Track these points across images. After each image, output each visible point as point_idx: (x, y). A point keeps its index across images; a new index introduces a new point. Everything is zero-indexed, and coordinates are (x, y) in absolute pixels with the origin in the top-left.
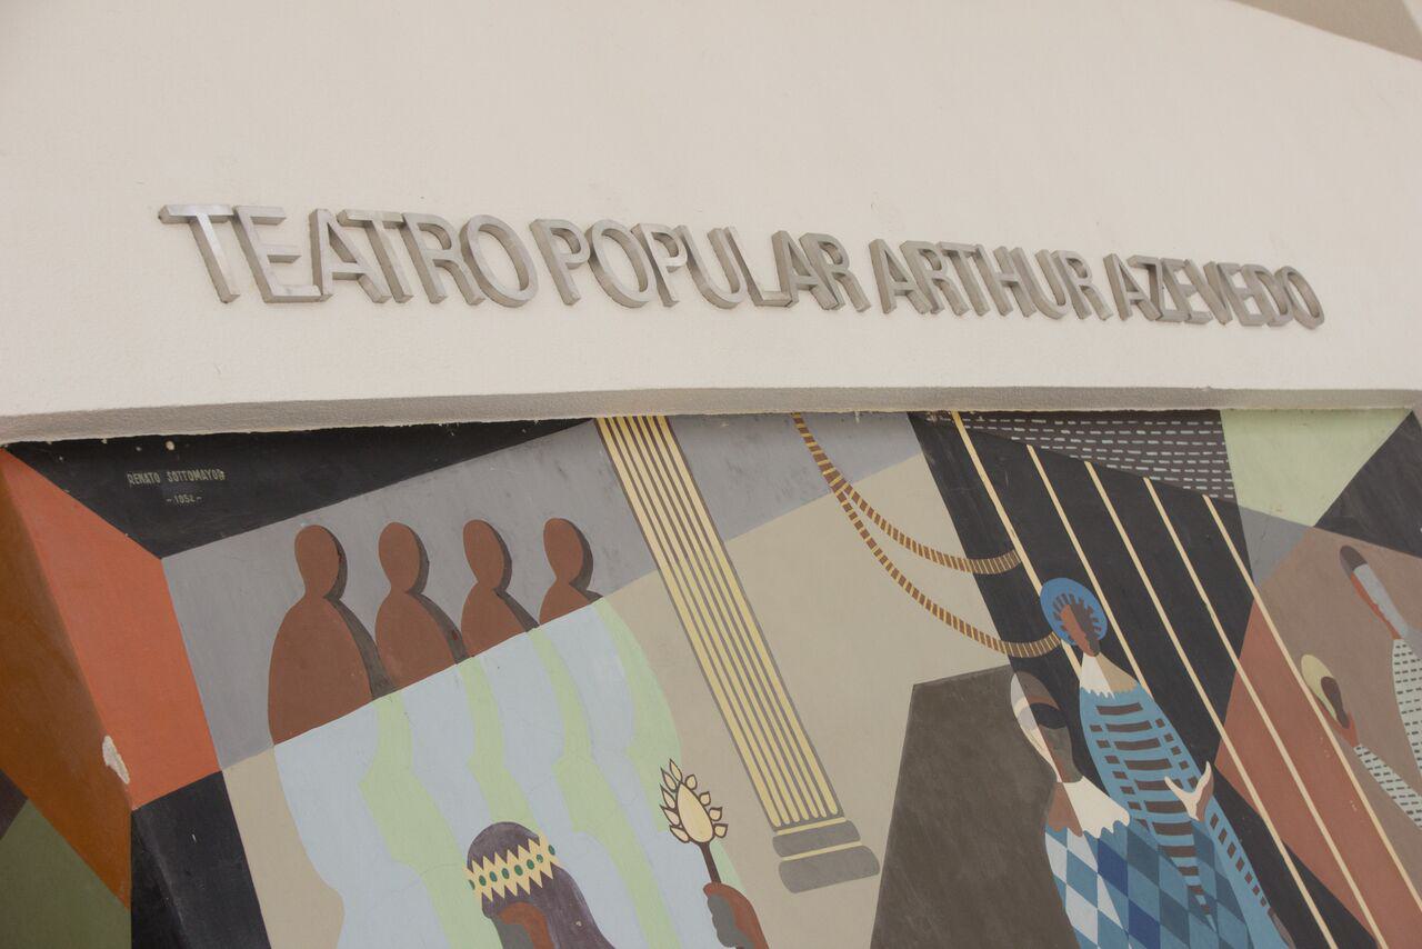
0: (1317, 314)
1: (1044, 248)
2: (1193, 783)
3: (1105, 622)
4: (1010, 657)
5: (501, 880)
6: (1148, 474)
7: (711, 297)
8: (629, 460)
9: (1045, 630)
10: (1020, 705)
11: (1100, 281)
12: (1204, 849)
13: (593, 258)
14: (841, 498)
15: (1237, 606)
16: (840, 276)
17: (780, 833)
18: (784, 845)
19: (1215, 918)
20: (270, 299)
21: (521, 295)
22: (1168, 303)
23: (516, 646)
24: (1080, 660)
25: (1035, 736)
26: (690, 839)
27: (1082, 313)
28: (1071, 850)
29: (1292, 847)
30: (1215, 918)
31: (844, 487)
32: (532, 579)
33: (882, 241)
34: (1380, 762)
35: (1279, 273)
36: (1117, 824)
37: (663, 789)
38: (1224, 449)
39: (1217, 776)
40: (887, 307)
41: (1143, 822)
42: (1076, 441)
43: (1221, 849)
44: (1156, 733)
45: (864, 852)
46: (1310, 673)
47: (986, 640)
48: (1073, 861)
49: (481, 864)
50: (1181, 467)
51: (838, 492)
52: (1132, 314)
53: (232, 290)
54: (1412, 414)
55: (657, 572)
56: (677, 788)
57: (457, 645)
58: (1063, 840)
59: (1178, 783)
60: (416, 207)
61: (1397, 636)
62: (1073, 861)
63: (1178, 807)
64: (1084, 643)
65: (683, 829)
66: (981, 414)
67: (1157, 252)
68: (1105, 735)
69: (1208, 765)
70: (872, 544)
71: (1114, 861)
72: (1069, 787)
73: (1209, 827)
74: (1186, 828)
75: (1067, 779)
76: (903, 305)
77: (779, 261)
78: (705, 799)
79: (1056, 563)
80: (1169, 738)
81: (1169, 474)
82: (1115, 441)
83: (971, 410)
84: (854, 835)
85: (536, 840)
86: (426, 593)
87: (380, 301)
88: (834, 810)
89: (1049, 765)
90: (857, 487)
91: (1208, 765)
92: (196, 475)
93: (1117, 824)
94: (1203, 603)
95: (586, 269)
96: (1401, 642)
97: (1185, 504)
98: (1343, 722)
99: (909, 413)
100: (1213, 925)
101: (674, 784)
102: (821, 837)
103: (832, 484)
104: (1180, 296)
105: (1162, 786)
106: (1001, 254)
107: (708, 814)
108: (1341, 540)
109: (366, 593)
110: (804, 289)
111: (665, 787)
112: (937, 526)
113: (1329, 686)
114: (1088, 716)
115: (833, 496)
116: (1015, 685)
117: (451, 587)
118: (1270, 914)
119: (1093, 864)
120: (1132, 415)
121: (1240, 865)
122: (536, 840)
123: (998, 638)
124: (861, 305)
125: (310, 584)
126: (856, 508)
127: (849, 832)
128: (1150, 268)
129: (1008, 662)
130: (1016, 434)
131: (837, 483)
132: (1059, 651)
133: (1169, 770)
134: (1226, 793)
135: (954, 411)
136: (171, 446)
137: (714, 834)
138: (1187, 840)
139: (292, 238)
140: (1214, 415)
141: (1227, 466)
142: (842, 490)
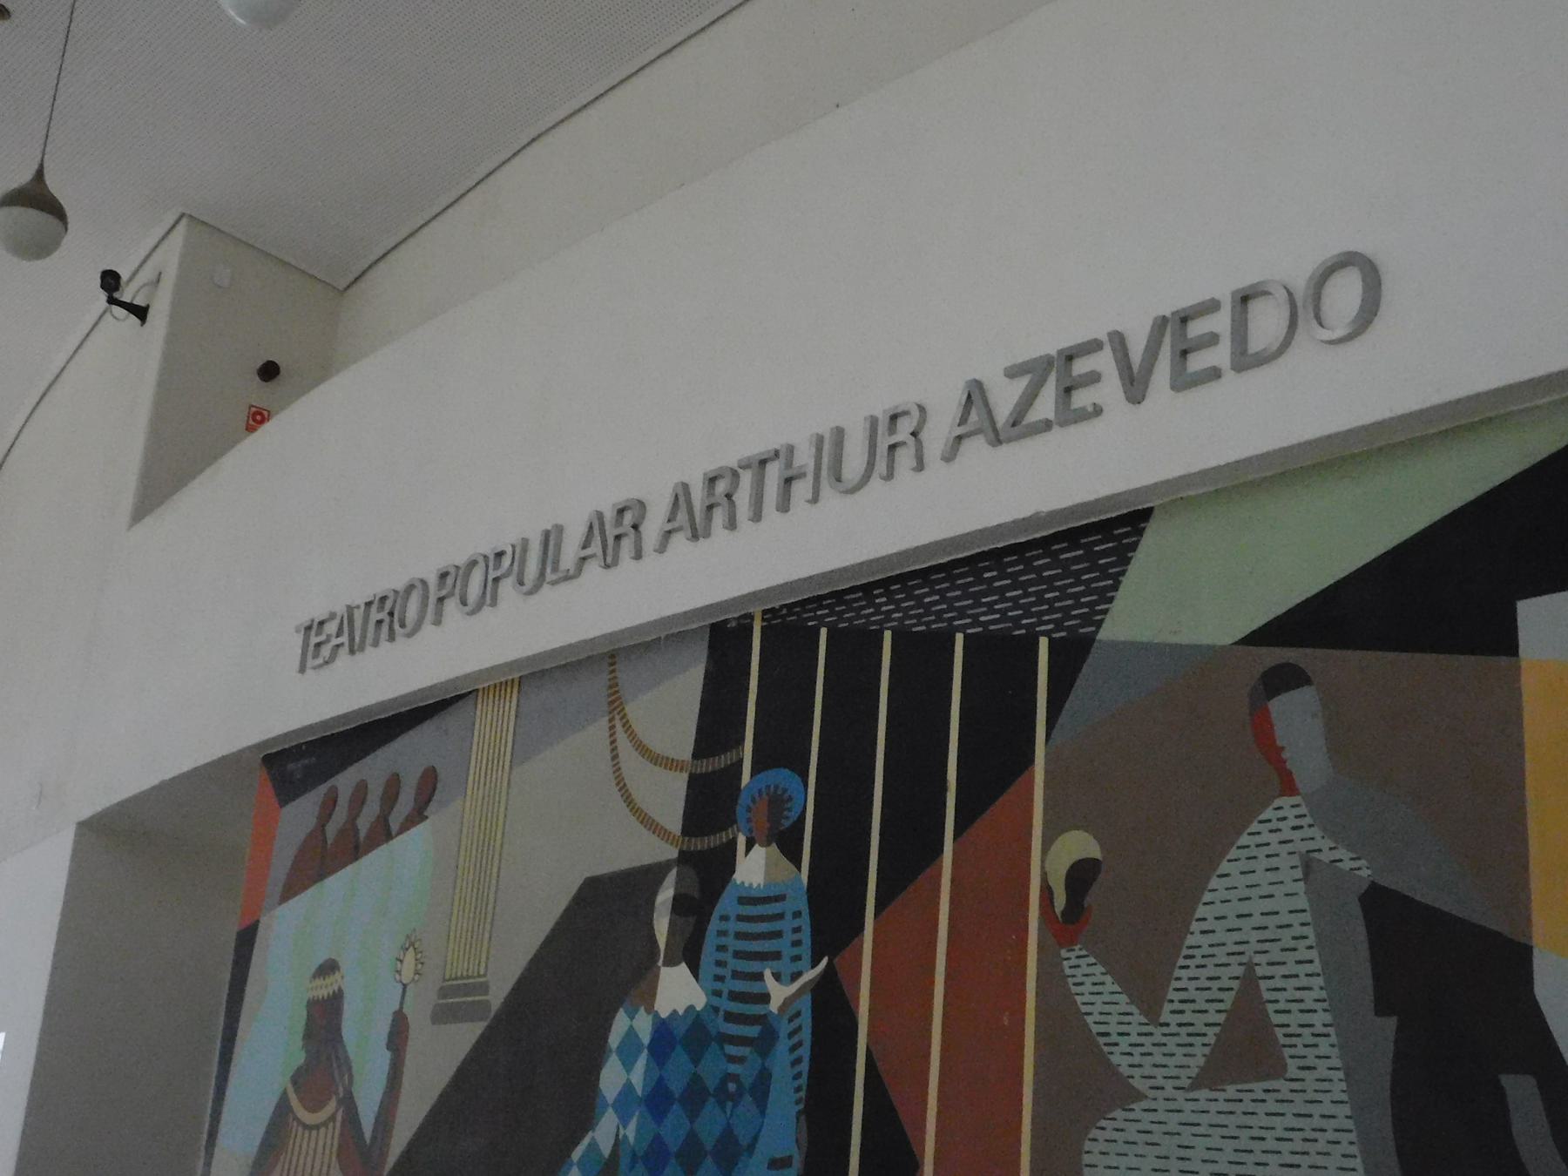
2: (795, 976)
3: (799, 811)
28: (634, 1026)
39: (829, 975)
43: (783, 1045)
45: (487, 1004)
48: (631, 1034)
52: (1234, 294)
61: (1289, 787)
62: (631, 1034)
63: (765, 998)
65: (400, 975)
69: (825, 961)
74: (761, 1019)
89: (659, 951)
100: (729, 1113)
101: (410, 944)
102: (468, 990)
127: (484, 988)
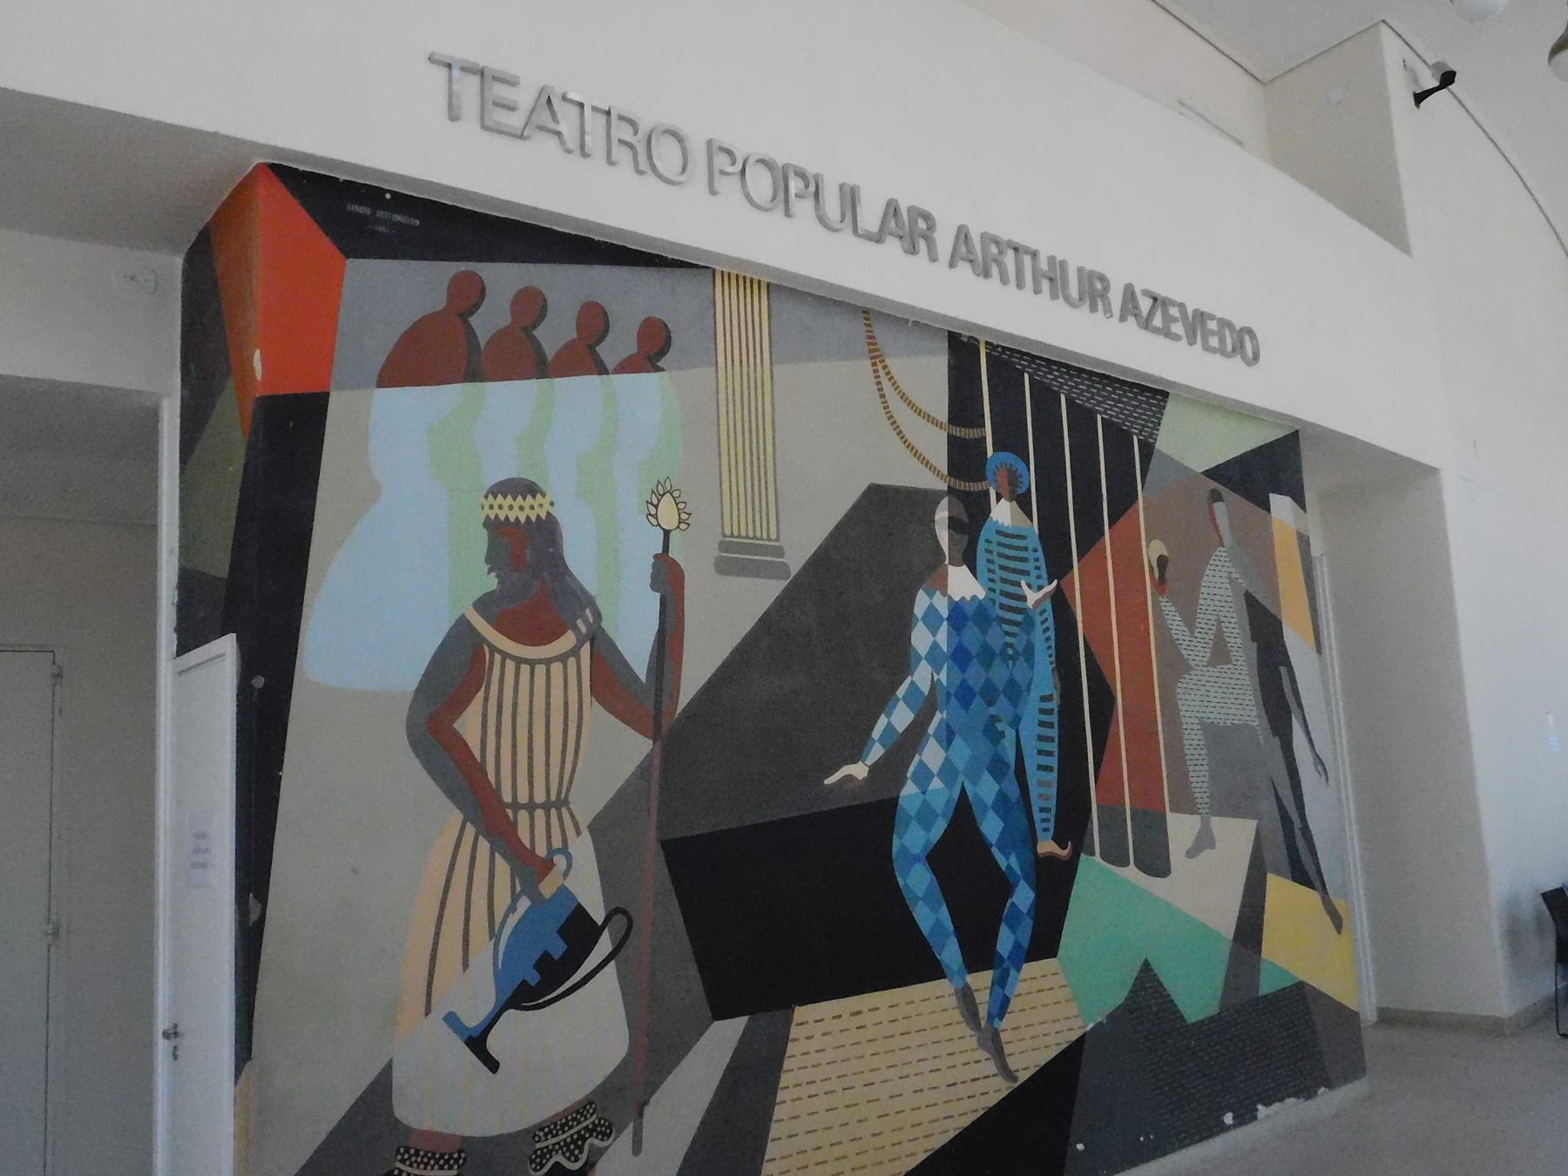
0: (1256, 357)
1: (1084, 265)
2: (1040, 588)
4: (949, 487)
5: (495, 504)
6: (1101, 413)
7: (822, 220)
8: (727, 301)
9: (982, 477)
10: (942, 514)
11: (1116, 297)
12: (1028, 624)
13: (743, 172)
14: (874, 364)
15: (1123, 500)
16: (925, 237)
17: (728, 539)
18: (725, 546)
19: (1014, 664)
20: (484, 127)
21: (681, 178)
22: (1157, 321)
23: (588, 384)
24: (998, 500)
25: (943, 535)
26: (659, 525)
27: (1093, 308)
29: (1091, 645)
30: (1014, 664)
31: (880, 359)
32: (620, 343)
33: (966, 226)
34: (1173, 609)
35: (1242, 329)
36: (974, 597)
37: (653, 491)
38: (1162, 414)
40: (1123, 318)
41: (993, 601)
42: (1104, 393)
43: (1039, 628)
44: (1029, 555)
46: (1152, 550)
47: (938, 473)
49: (495, 497)
50: (1127, 415)
51: (873, 361)
53: (791, 213)
54: (1297, 432)
55: (714, 369)
56: (664, 494)
57: (541, 368)
58: (931, 595)
59: (1029, 586)
60: (620, 106)
63: (1023, 598)
64: (1005, 487)
65: (657, 519)
66: (1001, 346)
67: (1162, 292)
68: (993, 547)
69: (1055, 582)
70: (882, 396)
71: (959, 615)
72: (951, 569)
73: (1037, 615)
75: (951, 563)
76: (1131, 320)
77: (957, 237)
78: (681, 506)
79: (1009, 439)
80: (1037, 560)
81: (1117, 417)
82: (1088, 388)
83: (995, 343)
84: (782, 555)
85: (544, 495)
86: (537, 333)
87: (569, 152)
88: (774, 536)
90: (888, 362)
91: (1055, 582)
92: (398, 218)
93: (974, 597)
94: (1102, 495)
95: (736, 181)
96: (1222, 549)
97: (1119, 438)
98: (1161, 583)
99: (949, 332)
101: (660, 492)
103: (872, 355)
104: (1168, 319)
105: (1019, 585)
106: (1052, 260)
107: (679, 515)
108: (1215, 485)
109: (489, 321)
110: (896, 237)
111: (655, 491)
112: (937, 400)
113: (1162, 562)
114: (986, 532)
115: (869, 362)
116: (945, 502)
117: (555, 334)
118: (1053, 670)
119: (945, 613)
120: (1118, 381)
121: (1048, 639)
122: (544, 495)
123: (946, 473)
124: (1108, 311)
125: (450, 301)
126: (882, 373)
127: (780, 552)
128: (1155, 299)
129: (946, 489)
130: (1021, 365)
131: (876, 355)
132: (987, 493)
133: (1027, 577)
134: (1060, 603)
135: (983, 339)
136: (388, 196)
137: (678, 527)
138: (1019, 618)
139: (524, 97)
140: (1166, 395)
141: (1159, 424)
142: (877, 360)
